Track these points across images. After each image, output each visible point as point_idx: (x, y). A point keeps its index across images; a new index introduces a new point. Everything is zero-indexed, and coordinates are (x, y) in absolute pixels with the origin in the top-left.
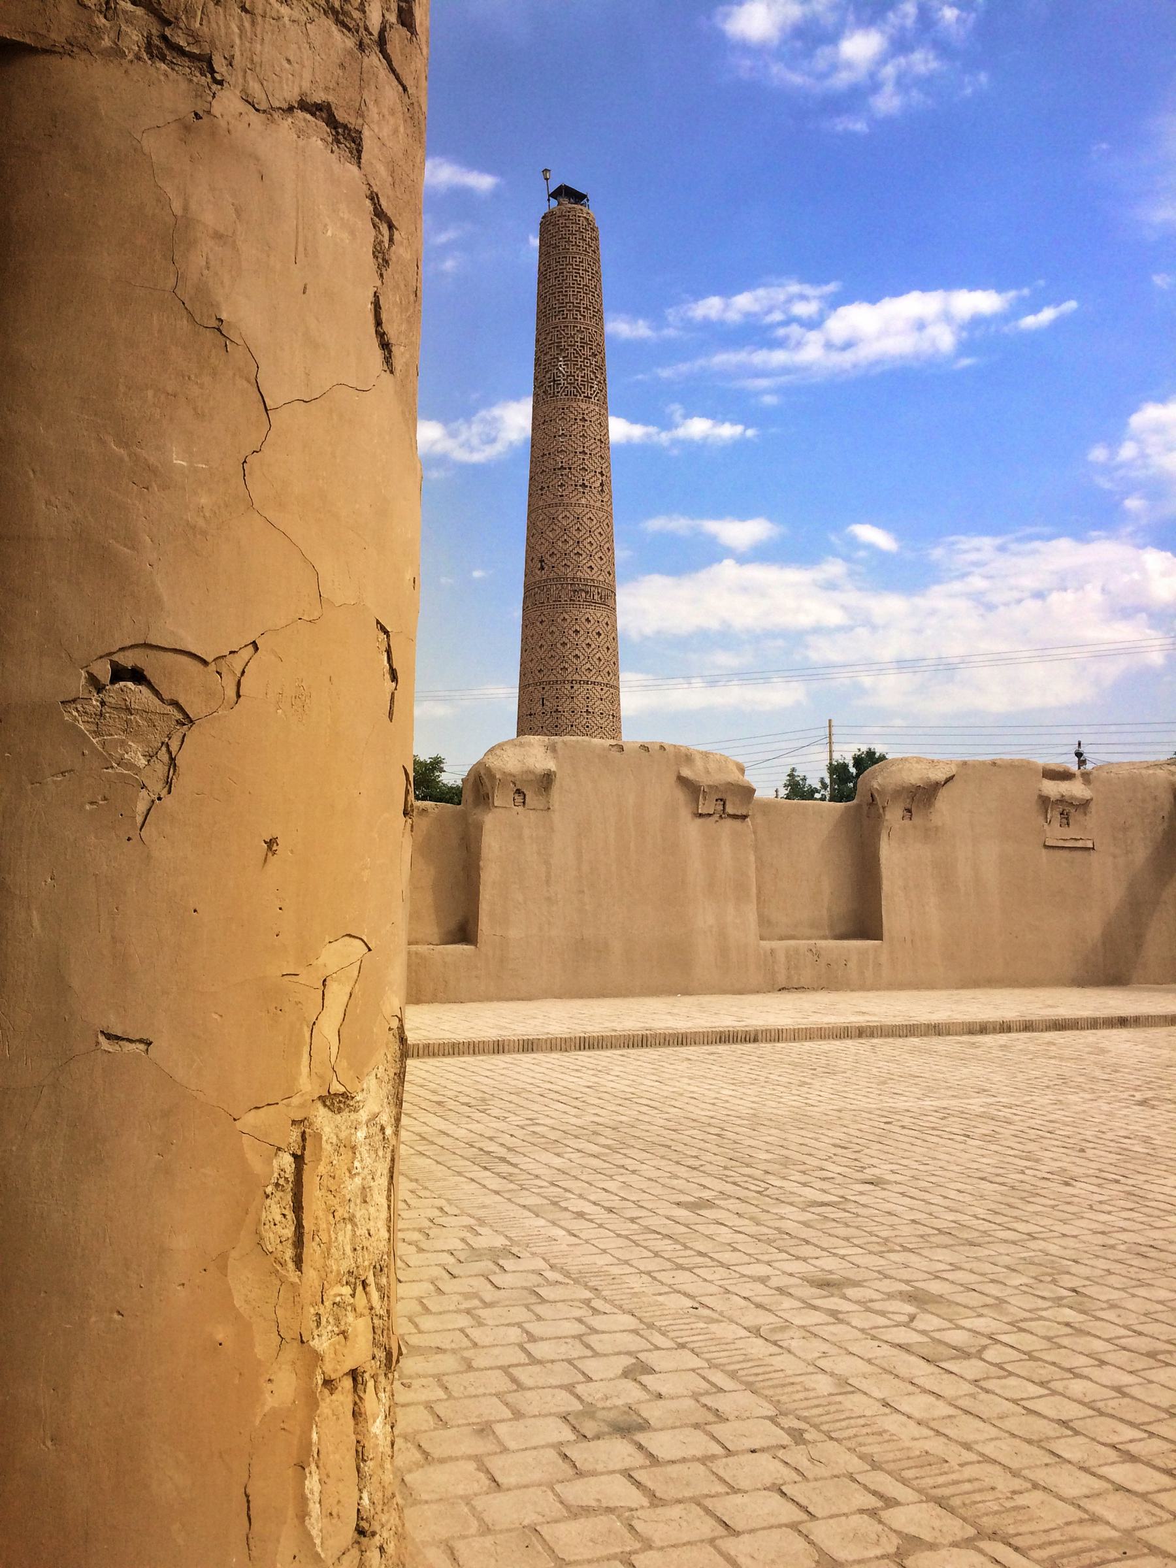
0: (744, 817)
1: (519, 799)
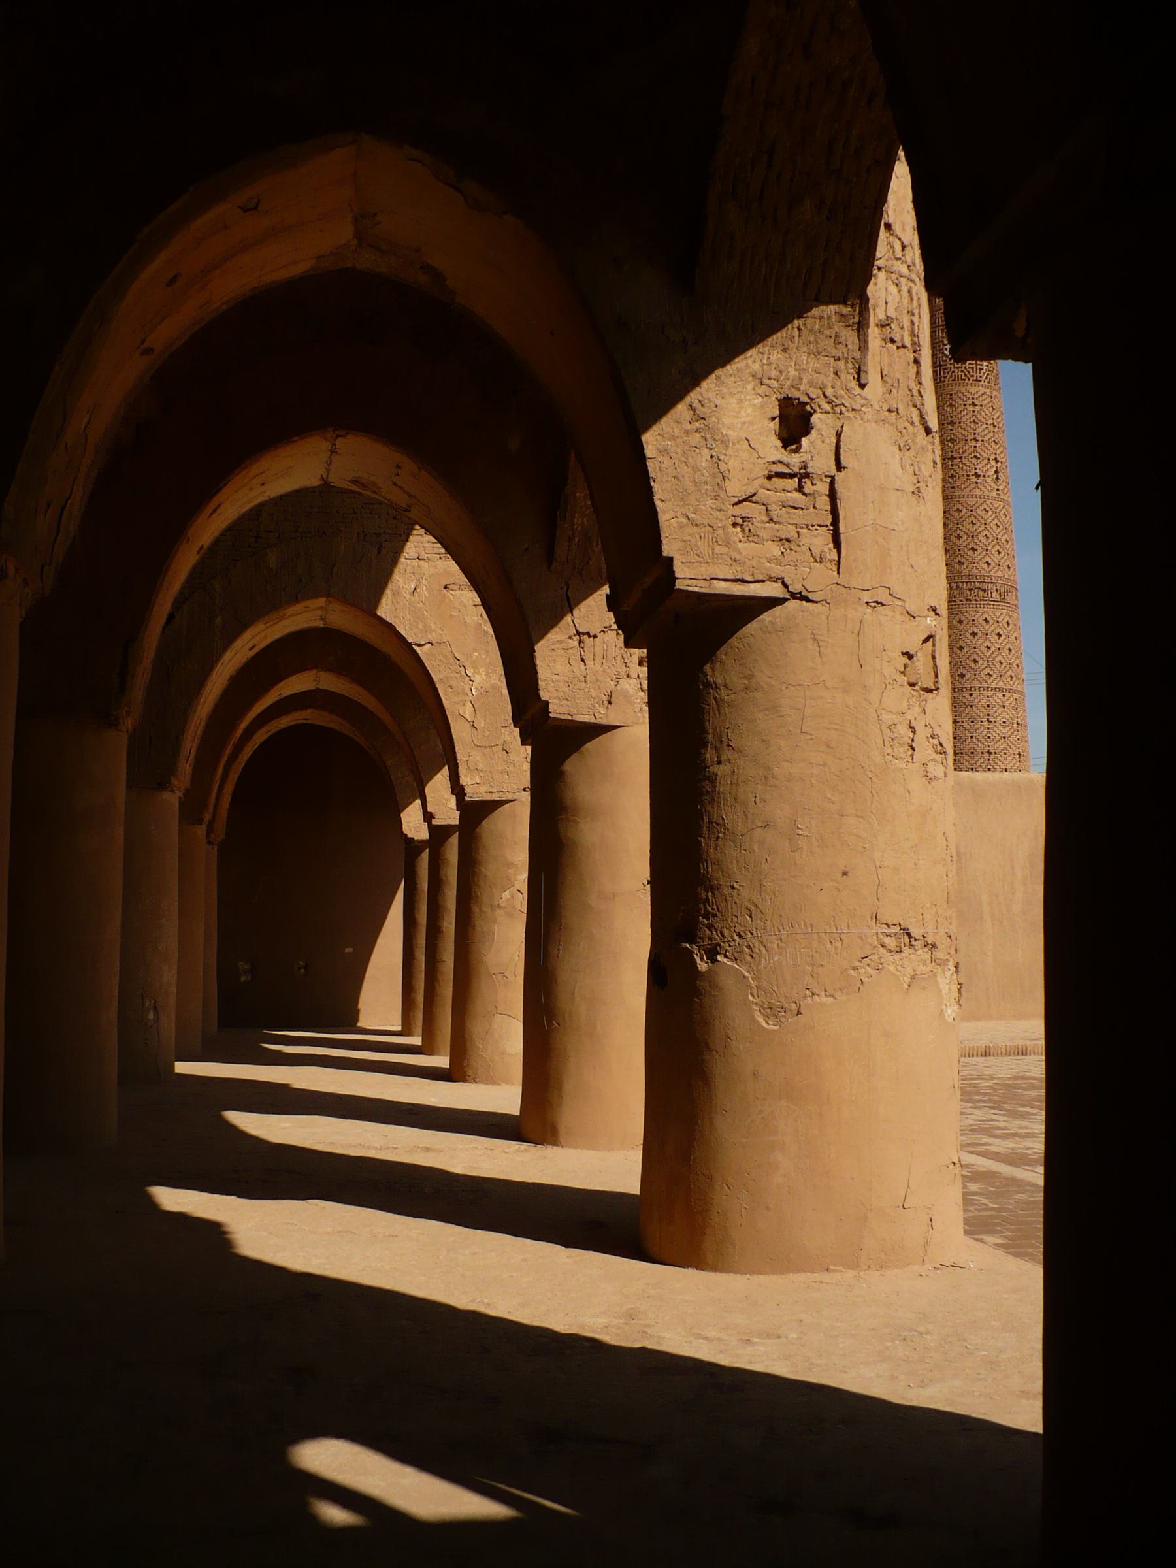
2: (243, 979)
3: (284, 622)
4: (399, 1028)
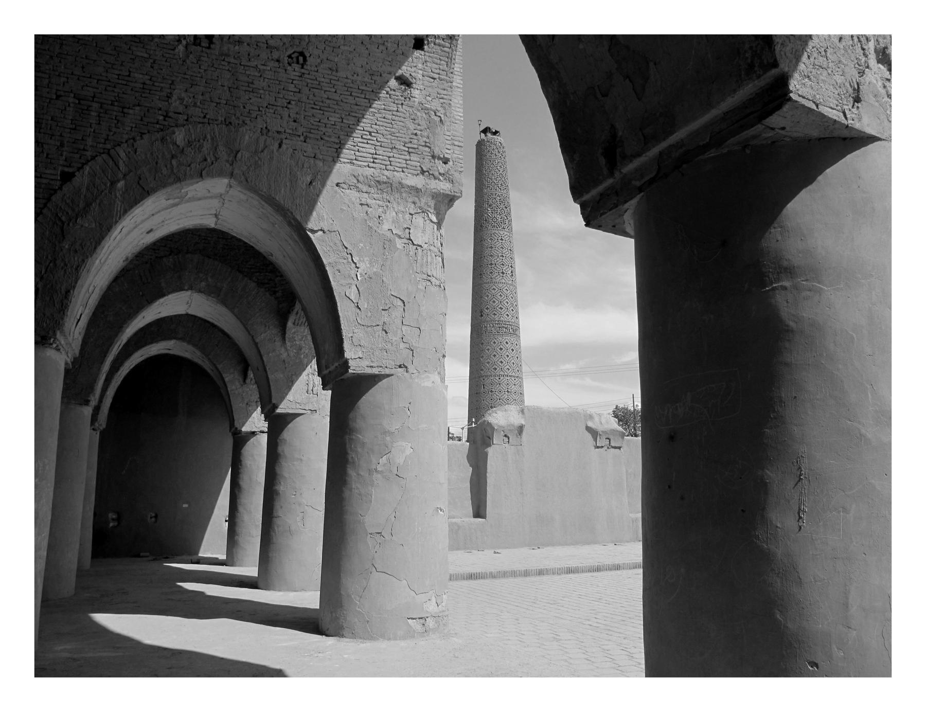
0: (619, 448)
1: (506, 439)
2: (111, 525)
3: (183, 208)
4: (224, 557)
